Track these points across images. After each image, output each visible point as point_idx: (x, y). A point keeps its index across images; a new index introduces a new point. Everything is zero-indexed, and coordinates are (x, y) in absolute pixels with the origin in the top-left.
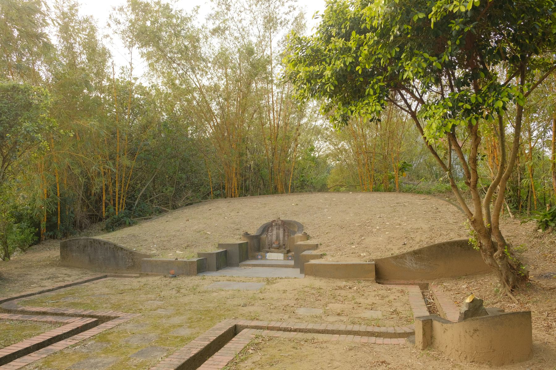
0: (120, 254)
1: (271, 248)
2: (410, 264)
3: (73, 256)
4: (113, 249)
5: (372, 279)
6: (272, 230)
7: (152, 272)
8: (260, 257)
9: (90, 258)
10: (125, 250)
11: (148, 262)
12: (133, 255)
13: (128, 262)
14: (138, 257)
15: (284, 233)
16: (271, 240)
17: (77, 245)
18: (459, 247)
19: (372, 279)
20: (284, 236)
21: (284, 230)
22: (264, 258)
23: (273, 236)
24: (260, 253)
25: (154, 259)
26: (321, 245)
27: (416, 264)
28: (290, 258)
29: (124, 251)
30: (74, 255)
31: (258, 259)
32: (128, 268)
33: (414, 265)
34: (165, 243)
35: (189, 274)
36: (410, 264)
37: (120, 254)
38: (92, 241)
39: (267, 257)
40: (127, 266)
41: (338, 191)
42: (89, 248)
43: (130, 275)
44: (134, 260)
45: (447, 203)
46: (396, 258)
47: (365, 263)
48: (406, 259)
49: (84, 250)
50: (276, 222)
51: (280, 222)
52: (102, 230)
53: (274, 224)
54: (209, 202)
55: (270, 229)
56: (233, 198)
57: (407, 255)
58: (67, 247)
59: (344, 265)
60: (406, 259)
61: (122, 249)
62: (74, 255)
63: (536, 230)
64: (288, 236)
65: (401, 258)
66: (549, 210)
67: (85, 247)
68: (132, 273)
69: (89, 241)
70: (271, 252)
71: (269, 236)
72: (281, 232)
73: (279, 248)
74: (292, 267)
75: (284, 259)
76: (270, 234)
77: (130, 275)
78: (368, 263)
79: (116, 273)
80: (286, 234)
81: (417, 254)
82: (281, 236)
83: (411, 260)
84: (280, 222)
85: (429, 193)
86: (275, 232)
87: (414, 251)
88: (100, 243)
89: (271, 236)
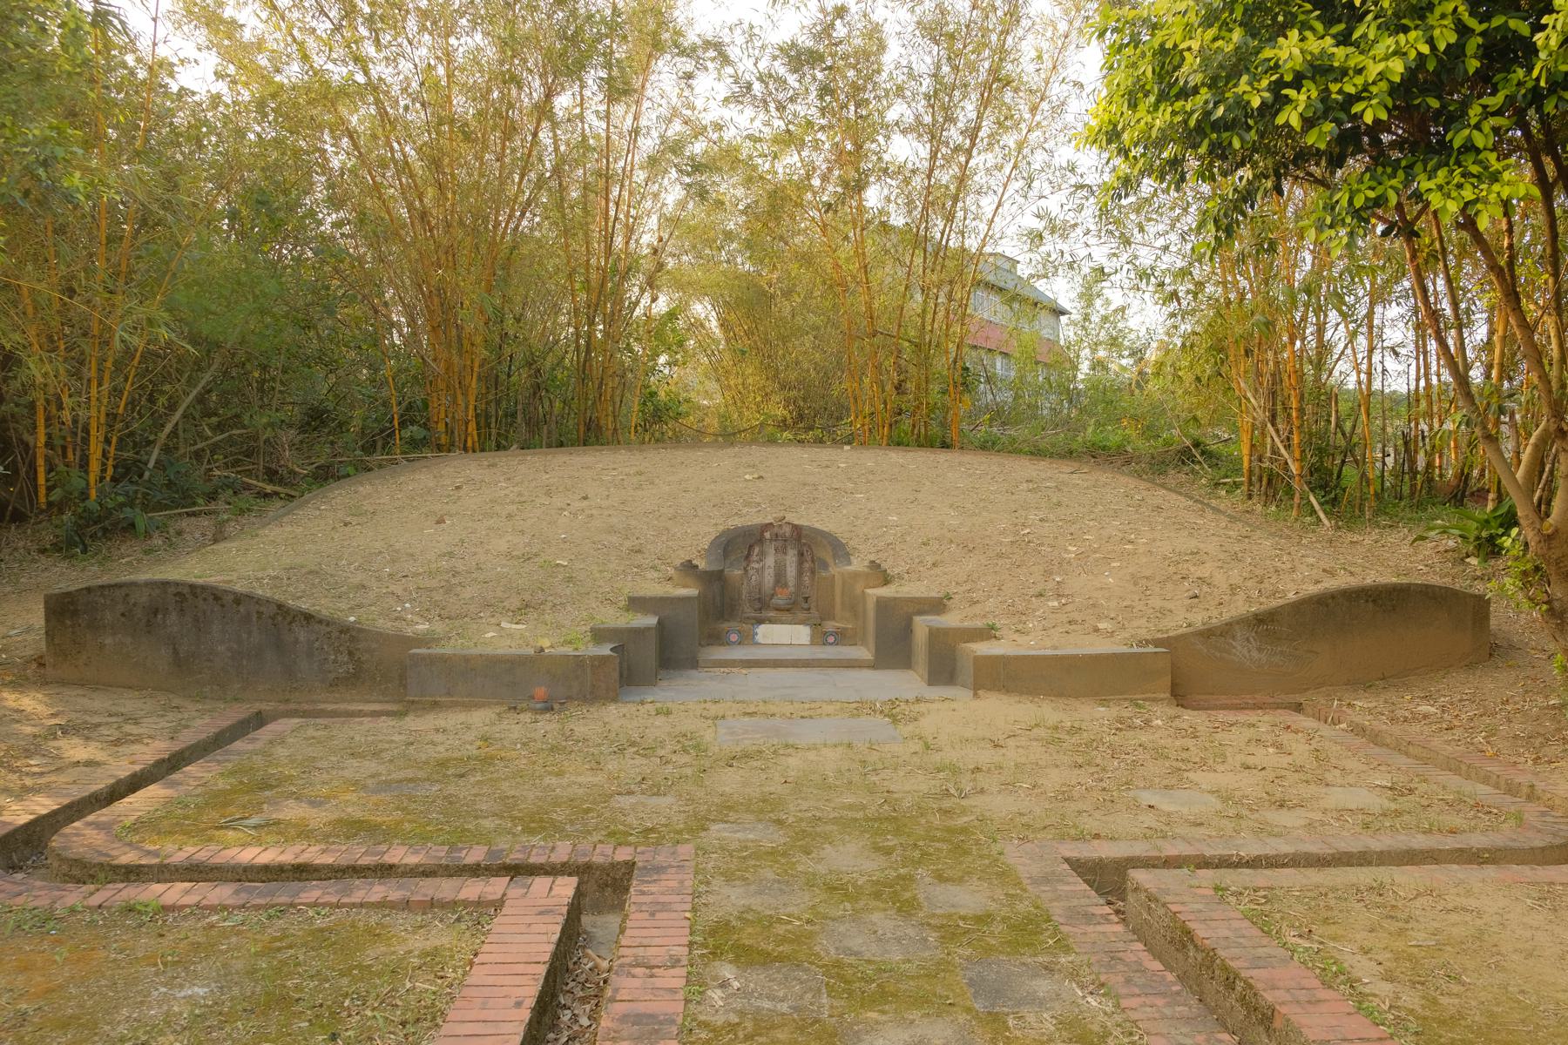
0: (302, 636)
1: (765, 608)
2: (1244, 650)
3: (102, 647)
4: (273, 618)
5: (1162, 696)
6: (762, 554)
7: (449, 694)
8: (734, 637)
9: (176, 652)
10: (320, 622)
11: (432, 660)
12: (353, 639)
13: (335, 661)
14: (374, 646)
15: (800, 563)
16: (760, 584)
17: (121, 608)
18: (1371, 605)
19: (1162, 696)
20: (800, 573)
21: (801, 554)
22: (748, 639)
23: (767, 572)
24: (734, 625)
25: (437, 650)
26: (223, 606)
27: (1260, 650)
28: (831, 639)
29: (317, 627)
30: (109, 641)
31: (729, 643)
32: (335, 684)
33: (1255, 654)
34: (437, 597)
35: (593, 696)
36: (1245, 651)
37: (302, 636)
38: (186, 590)
39: (759, 638)
40: (332, 676)
41: (772, 441)
42: (174, 617)
43: (342, 707)
44: (358, 655)
45: (1149, 485)
46: (1208, 634)
47: (1125, 649)
48: (1234, 637)
49: (148, 622)
50: (776, 530)
51: (787, 530)
52: (43, 551)
53: (767, 535)
54: (423, 462)
55: (757, 550)
56: (479, 454)
57: (1237, 627)
58: (75, 613)
59: (1090, 656)
60: (1234, 637)
61: (308, 617)
62: (109, 641)
63: (1462, 560)
64: (813, 572)
65: (1221, 635)
66: (1495, 510)
67: (156, 613)
68: (353, 701)
69: (172, 590)
70: (771, 621)
71: (751, 572)
72: (791, 559)
73: (793, 609)
74: (868, 667)
75: (813, 643)
76: (756, 566)
77: (342, 707)
78: (1135, 650)
79: (287, 701)
80: (807, 565)
81: (1263, 623)
82: (791, 572)
83: (1248, 639)
84: (787, 530)
85: (1069, 454)
86: (770, 561)
87: (1256, 615)
88: (217, 598)
89: (760, 571)
